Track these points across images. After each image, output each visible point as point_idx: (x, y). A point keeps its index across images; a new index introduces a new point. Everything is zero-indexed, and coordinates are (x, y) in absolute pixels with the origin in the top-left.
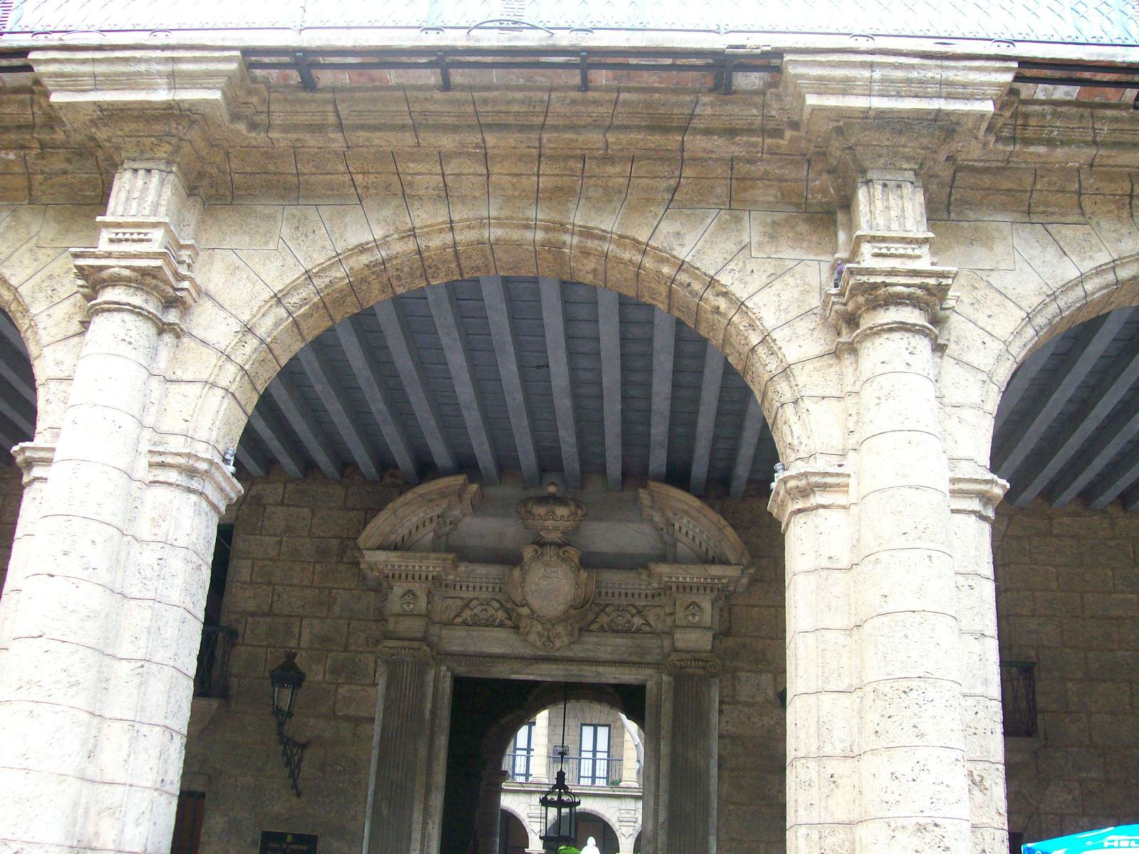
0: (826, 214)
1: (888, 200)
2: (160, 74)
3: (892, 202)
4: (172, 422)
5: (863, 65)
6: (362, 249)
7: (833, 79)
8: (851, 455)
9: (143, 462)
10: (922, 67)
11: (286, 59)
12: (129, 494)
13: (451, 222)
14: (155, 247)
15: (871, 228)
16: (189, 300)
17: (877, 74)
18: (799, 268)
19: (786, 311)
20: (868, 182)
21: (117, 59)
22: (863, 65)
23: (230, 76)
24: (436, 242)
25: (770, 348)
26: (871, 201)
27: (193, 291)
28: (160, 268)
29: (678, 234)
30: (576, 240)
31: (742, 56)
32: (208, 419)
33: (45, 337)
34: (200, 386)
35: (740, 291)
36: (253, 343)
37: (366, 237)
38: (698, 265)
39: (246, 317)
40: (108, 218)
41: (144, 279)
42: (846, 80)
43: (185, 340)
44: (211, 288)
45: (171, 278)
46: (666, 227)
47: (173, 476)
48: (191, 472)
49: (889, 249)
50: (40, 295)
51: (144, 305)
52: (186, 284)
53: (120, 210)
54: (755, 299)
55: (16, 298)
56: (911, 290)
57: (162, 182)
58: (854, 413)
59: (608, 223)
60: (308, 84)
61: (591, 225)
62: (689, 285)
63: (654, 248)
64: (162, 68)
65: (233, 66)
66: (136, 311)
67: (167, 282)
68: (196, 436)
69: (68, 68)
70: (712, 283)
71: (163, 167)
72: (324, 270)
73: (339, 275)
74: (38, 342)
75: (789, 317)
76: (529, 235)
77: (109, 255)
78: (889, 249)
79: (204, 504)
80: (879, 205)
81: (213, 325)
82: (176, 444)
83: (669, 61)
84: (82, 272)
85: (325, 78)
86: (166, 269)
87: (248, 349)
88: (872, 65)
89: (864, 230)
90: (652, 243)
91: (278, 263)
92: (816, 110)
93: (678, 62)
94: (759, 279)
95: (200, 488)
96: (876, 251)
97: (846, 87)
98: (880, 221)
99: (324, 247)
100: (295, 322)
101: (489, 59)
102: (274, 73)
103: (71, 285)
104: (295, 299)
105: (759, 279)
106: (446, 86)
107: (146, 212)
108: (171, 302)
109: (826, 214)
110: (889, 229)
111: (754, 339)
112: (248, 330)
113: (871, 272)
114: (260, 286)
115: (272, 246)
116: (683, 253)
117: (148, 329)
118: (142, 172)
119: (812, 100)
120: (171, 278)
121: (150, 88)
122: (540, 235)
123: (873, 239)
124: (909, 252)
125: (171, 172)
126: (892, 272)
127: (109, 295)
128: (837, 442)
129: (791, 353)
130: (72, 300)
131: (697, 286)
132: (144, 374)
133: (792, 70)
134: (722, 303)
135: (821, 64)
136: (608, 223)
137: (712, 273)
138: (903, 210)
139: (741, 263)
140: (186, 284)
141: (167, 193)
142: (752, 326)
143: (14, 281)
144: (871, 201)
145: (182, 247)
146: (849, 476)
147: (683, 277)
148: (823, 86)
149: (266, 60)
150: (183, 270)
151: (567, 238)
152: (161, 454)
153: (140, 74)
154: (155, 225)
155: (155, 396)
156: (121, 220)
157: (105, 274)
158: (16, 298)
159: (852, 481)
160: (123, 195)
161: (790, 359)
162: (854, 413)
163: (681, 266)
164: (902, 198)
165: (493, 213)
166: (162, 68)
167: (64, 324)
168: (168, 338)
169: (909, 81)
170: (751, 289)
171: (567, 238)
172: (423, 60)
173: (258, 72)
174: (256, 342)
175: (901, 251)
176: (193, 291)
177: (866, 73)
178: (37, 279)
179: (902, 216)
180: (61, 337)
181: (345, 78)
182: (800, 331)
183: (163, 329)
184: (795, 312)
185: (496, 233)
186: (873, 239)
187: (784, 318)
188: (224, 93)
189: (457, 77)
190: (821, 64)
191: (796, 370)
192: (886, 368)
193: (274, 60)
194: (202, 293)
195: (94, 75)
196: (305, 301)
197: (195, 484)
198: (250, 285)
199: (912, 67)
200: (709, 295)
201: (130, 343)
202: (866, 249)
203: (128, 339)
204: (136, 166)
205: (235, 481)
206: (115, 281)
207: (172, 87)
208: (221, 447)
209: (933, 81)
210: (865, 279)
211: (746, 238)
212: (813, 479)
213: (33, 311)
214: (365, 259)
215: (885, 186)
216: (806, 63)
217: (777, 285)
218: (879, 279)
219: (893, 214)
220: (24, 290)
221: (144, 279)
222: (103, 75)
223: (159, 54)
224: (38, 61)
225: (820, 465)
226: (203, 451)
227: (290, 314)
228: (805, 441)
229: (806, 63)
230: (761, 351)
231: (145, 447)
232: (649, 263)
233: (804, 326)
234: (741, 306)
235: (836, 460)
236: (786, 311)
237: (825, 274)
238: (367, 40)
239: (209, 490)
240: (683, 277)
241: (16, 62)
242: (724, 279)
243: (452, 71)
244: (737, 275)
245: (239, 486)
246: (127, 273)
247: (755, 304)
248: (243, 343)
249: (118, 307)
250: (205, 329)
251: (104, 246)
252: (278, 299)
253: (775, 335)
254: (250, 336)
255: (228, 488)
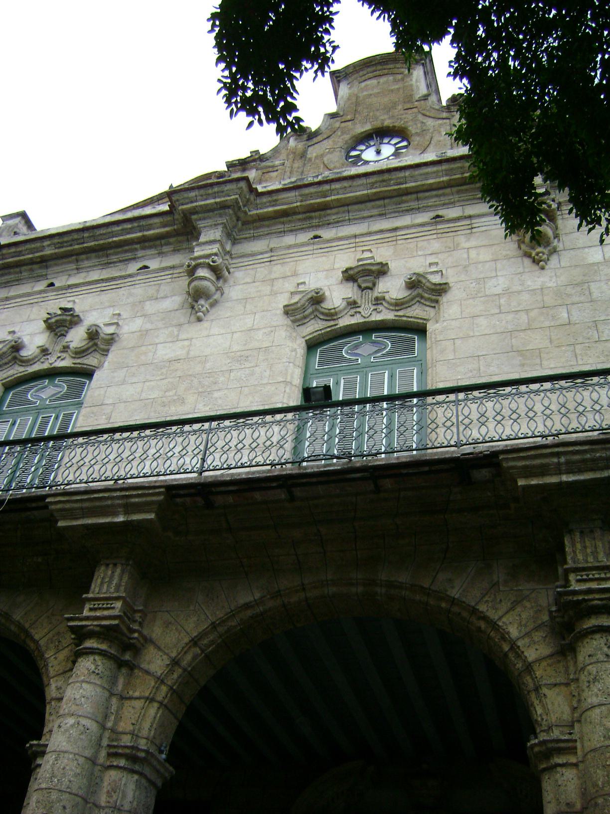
0: (543, 559)
1: (584, 542)
2: (119, 505)
3: (588, 544)
4: (124, 726)
5: (553, 455)
6: (247, 606)
7: (534, 467)
8: (576, 725)
9: (103, 753)
10: (593, 451)
11: (193, 491)
12: (92, 774)
13: (303, 584)
14: (116, 612)
15: (574, 562)
16: (139, 645)
17: (562, 460)
18: (533, 595)
19: (525, 626)
20: (570, 532)
21: (95, 498)
22: (553, 455)
23: (159, 503)
24: (294, 599)
25: (517, 653)
26: (573, 545)
27: (141, 639)
28: (117, 625)
29: (450, 580)
30: (384, 590)
31: (471, 459)
32: (143, 720)
33: (52, 672)
34: (143, 701)
35: (493, 615)
36: (178, 672)
37: (250, 599)
38: (464, 599)
39: (174, 655)
40: (90, 595)
41: (106, 634)
42: (542, 466)
43: (136, 671)
44: (154, 636)
45: (125, 631)
46: (442, 576)
47: (122, 762)
48: (133, 759)
49: (588, 575)
50: (52, 645)
51: (109, 650)
52: (136, 635)
53: (97, 590)
54: (504, 619)
55: (37, 648)
56: (604, 602)
57: (123, 572)
58: (576, 694)
59: (404, 578)
60: (209, 505)
61: (393, 579)
62: (460, 614)
63: (436, 591)
64: (120, 502)
65: (162, 497)
66: (101, 653)
67: (123, 634)
68: (140, 735)
69: (68, 506)
70: (474, 611)
71: (123, 562)
72: (223, 621)
73: (233, 624)
74: (48, 676)
75: (528, 630)
76: (354, 590)
77: (87, 618)
78: (588, 575)
79: (144, 781)
80: (579, 546)
81: (155, 662)
82: (126, 740)
83: (427, 469)
84: (73, 629)
85: (219, 500)
86: (121, 626)
87: (175, 676)
88: (558, 455)
89: (570, 564)
90: (433, 588)
91: (195, 619)
92: (524, 487)
93: (433, 468)
94: (505, 606)
95: (140, 770)
96: (579, 577)
97: (543, 471)
98: (580, 557)
99: (223, 607)
100: (207, 656)
101: (314, 480)
102: (188, 499)
103: (70, 637)
104: (205, 642)
105: (505, 606)
106: (292, 499)
107: (112, 590)
108: (127, 646)
109: (546, 561)
110: (587, 562)
111: (506, 648)
112: (175, 663)
113: (575, 593)
114: (183, 634)
115: (192, 608)
116: (455, 593)
117: (109, 664)
118: (111, 566)
119: (521, 482)
120: (125, 631)
121: (115, 514)
122: (360, 589)
123: (576, 570)
124: (603, 576)
125: (128, 565)
126: (590, 591)
127: (90, 643)
128: (566, 715)
129: (531, 655)
130: (70, 647)
131: (465, 614)
132: (107, 694)
133: (505, 465)
134: (483, 625)
135: (524, 458)
136: (404, 578)
137: (473, 604)
138: (596, 548)
139: (493, 596)
140: (136, 635)
141: (126, 578)
142: (503, 638)
143: (37, 637)
144: (573, 545)
145: (136, 611)
146: (576, 741)
147: (455, 609)
148: (529, 472)
149: (182, 492)
150: (136, 627)
151: (378, 589)
152: (115, 747)
153: (108, 506)
154: (117, 599)
155: (114, 708)
156: (98, 596)
157: (85, 630)
158: (37, 648)
159: (578, 745)
160: (99, 581)
161: (530, 659)
162: (576, 694)
163: (453, 601)
164: (594, 539)
165: (329, 577)
166: (120, 502)
167: (64, 663)
168: (124, 670)
169: (584, 461)
170: (500, 613)
171: (378, 589)
172: (274, 484)
173: (178, 500)
174: (180, 670)
175: (597, 576)
176: (141, 639)
177: (555, 460)
178: (50, 635)
179: (595, 553)
180: (61, 671)
181: (230, 499)
182: (536, 639)
183: (120, 664)
184: (531, 626)
185: (333, 590)
186: (576, 570)
187: (524, 630)
188: (157, 515)
189: (298, 492)
190: (524, 458)
191: (535, 667)
192: (594, 659)
193: (186, 492)
194: (148, 640)
195: (82, 509)
196: (212, 642)
197: (137, 767)
198: (177, 634)
199: (585, 451)
200: (473, 619)
201: (98, 674)
202: (572, 577)
203: (97, 671)
204: (108, 562)
205: (167, 765)
206: (91, 635)
207: (126, 513)
208: (158, 742)
209: (601, 458)
210: (570, 598)
211: (495, 578)
212: (550, 745)
213: (47, 656)
214: (249, 613)
215: (582, 532)
216: (514, 459)
217: (518, 609)
218: (580, 598)
219: (589, 551)
220: (42, 643)
221: (106, 634)
222: (87, 508)
223: (118, 494)
224: (51, 503)
225: (556, 734)
226: (143, 744)
227: (203, 651)
228: (545, 717)
229: (514, 459)
230: (511, 656)
231: (105, 742)
232: (432, 602)
233: (538, 636)
234: (494, 625)
235: (567, 730)
236: (525, 626)
237: (551, 599)
238: (148, 419)
239: (147, 771)
240: (455, 609)
241: (41, 504)
242: (482, 608)
243: (293, 489)
244: (490, 605)
245: (171, 768)
246: (97, 629)
247: (504, 623)
248: (171, 671)
249: (91, 652)
250: (149, 663)
251: (86, 613)
252: (194, 642)
253: (519, 643)
254: (176, 668)
255: (162, 770)
